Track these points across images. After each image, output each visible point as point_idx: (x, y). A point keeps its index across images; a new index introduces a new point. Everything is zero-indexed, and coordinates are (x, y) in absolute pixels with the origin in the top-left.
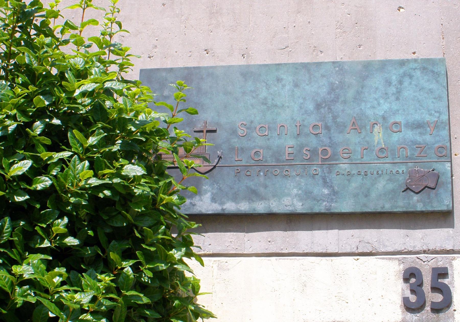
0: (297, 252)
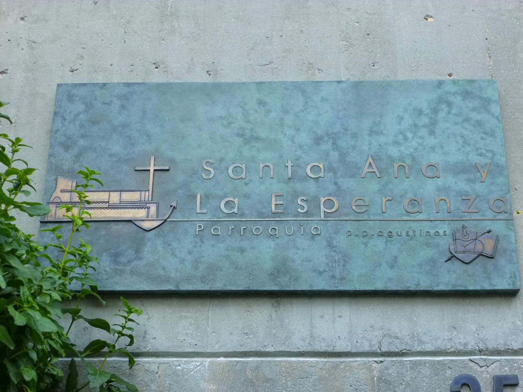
0: (288, 350)
